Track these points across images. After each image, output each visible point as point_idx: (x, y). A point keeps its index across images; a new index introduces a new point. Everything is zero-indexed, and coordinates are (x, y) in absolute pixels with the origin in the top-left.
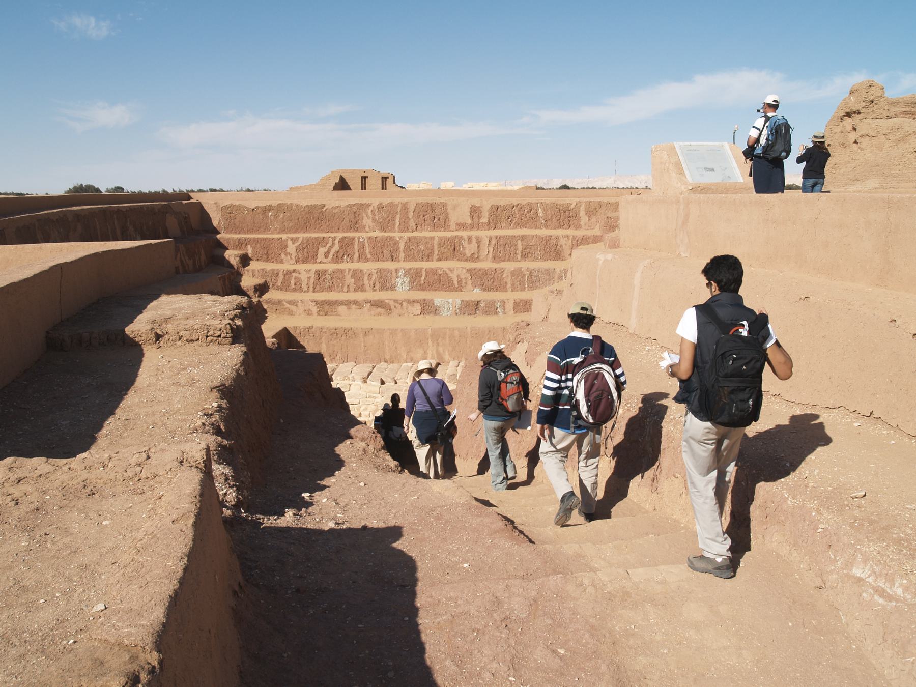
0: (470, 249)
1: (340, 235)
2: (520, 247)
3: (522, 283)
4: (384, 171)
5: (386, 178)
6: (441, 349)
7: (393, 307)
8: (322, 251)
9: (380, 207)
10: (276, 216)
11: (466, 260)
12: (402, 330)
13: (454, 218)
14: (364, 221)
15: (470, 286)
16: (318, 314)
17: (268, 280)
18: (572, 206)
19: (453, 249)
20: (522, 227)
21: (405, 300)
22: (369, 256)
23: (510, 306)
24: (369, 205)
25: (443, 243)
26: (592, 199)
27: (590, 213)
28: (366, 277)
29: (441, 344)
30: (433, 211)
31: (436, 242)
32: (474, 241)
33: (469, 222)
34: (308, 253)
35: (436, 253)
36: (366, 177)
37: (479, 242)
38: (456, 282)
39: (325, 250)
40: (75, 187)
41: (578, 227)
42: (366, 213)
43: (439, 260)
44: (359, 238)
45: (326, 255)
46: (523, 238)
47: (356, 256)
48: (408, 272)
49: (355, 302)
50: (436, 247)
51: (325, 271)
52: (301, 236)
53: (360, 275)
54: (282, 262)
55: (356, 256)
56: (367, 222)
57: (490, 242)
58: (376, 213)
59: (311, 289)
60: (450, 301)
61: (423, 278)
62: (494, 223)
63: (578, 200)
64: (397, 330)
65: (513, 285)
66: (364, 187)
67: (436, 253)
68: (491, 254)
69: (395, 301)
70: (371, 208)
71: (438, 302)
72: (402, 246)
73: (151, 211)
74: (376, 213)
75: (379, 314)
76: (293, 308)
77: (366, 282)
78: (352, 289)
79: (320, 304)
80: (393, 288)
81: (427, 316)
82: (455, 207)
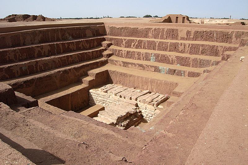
0: (181, 48)
1: (138, 39)
2: (201, 49)
3: (196, 64)
4: (184, 14)
5: (184, 18)
6: (153, 87)
7: (145, 67)
8: (133, 44)
9: (155, 29)
10: (124, 31)
11: (179, 52)
12: (141, 77)
13: (180, 35)
14: (149, 34)
15: (176, 63)
16: (123, 66)
17: (114, 52)
18: (230, 33)
19: (175, 48)
20: (206, 40)
21: (149, 66)
22: (146, 48)
23: (187, 74)
24: (152, 29)
25: (172, 44)
26: (239, 30)
27: (237, 37)
28: (142, 55)
29: (153, 85)
30: (173, 32)
31: (169, 44)
32: (183, 45)
33: (186, 37)
34: (128, 45)
35: (169, 48)
36: (178, 17)
37: (185, 46)
38: (171, 61)
39: (133, 44)
40: (146, 16)
41: (230, 43)
42: (150, 31)
43: (170, 51)
44: (144, 41)
45: (134, 45)
46: (202, 45)
47: (142, 47)
48: (155, 54)
49: (134, 64)
50: (169, 46)
51: (130, 51)
52: (128, 38)
53: (140, 54)
54: (121, 47)
55: (142, 47)
56: (150, 35)
57: (189, 46)
58: (154, 32)
59: (125, 57)
60: (165, 68)
61: (160, 58)
62: (195, 38)
63: (232, 30)
64: (139, 77)
65: (193, 65)
66: (177, 22)
67: (169, 48)
68: (189, 51)
69: (146, 65)
70: (152, 30)
71: (160, 68)
72: (157, 45)
73: (79, 29)
74: (154, 32)
75: (141, 69)
76: (116, 63)
77: (141, 57)
78: (137, 59)
79: (124, 63)
80: (149, 60)
81: (156, 72)
82: (181, 31)
